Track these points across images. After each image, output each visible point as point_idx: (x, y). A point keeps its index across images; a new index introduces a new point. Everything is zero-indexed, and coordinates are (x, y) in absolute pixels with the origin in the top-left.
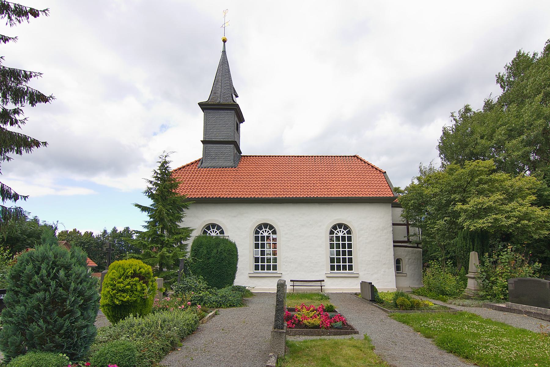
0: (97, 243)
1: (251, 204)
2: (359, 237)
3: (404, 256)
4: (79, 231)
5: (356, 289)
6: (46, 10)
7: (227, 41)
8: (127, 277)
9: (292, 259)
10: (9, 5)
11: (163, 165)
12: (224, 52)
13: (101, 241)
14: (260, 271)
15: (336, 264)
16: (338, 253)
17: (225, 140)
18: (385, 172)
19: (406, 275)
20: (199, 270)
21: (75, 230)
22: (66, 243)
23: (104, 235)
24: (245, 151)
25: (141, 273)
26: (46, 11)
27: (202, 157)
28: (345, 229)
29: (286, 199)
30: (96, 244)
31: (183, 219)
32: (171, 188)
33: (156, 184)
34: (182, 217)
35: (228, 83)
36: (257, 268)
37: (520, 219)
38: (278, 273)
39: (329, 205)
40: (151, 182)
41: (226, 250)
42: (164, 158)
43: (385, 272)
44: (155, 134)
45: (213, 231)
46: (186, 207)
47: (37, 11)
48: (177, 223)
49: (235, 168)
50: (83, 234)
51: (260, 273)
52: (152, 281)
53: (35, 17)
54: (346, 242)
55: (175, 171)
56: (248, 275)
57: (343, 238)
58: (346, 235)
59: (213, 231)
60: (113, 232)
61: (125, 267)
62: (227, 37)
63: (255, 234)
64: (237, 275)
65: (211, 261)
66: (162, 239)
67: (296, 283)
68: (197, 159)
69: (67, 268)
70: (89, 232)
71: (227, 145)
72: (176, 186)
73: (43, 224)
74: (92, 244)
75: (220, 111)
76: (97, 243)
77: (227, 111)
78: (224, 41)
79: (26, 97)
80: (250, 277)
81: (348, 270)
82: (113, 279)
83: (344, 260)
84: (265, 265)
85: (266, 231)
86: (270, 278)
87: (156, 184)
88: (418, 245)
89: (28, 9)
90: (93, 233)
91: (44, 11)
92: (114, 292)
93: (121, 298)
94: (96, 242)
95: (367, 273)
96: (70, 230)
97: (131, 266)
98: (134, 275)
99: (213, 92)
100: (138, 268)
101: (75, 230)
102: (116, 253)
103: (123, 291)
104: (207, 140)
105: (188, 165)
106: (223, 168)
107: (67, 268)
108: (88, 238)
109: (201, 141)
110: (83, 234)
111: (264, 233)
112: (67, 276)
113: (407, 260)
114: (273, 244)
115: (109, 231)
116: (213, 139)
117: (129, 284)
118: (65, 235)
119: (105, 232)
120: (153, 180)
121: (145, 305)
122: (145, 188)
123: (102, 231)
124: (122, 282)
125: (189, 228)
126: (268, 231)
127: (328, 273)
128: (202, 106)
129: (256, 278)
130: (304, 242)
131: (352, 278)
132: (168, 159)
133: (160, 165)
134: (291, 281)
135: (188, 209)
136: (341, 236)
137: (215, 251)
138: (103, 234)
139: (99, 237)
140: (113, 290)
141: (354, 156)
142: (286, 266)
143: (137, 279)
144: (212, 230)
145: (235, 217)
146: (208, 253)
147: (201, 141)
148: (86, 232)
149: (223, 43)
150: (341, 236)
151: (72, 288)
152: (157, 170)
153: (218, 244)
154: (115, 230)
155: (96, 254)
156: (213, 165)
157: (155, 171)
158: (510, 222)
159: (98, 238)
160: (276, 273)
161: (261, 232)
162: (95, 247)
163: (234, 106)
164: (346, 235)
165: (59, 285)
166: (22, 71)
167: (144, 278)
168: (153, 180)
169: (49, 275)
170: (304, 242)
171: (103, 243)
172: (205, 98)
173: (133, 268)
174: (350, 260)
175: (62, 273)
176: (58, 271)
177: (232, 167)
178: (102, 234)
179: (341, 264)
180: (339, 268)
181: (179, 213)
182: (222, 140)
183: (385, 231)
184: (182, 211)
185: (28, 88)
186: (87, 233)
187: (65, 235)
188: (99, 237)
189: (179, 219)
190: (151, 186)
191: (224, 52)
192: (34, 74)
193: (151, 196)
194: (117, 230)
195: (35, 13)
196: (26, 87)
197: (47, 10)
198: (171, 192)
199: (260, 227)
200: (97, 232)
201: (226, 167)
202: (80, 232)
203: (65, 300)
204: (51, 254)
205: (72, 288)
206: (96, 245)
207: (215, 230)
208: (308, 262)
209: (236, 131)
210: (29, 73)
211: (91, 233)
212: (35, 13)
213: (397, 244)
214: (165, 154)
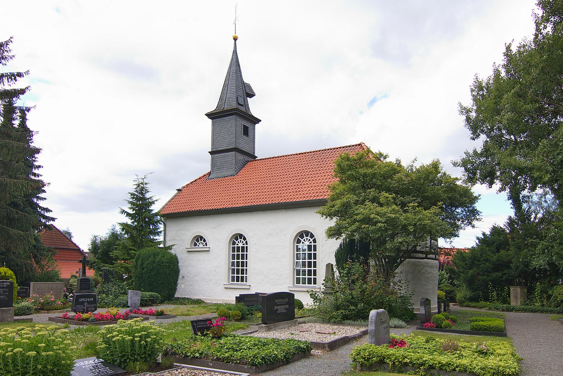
1: (258, 212)
6: (28, 87)
7: (238, 39)
9: (259, 271)
12: (235, 52)
14: (301, 285)
19: (248, 287)
24: (260, 153)
29: (251, 207)
35: (234, 86)
38: (317, 287)
39: (294, 211)
44: (362, 113)
62: (237, 35)
63: (232, 245)
77: (229, 117)
78: (235, 39)
80: (225, 288)
84: (300, 278)
111: (305, 241)
114: (304, 255)
127: (226, 284)
128: (209, 115)
129: (230, 289)
131: (232, 289)
136: (241, 247)
141: (359, 145)
142: (254, 278)
144: (305, 238)
149: (234, 41)
150: (241, 247)
163: (234, 111)
164: (312, 244)
172: (212, 107)
191: (235, 52)
201: (227, 176)
208: (273, 274)
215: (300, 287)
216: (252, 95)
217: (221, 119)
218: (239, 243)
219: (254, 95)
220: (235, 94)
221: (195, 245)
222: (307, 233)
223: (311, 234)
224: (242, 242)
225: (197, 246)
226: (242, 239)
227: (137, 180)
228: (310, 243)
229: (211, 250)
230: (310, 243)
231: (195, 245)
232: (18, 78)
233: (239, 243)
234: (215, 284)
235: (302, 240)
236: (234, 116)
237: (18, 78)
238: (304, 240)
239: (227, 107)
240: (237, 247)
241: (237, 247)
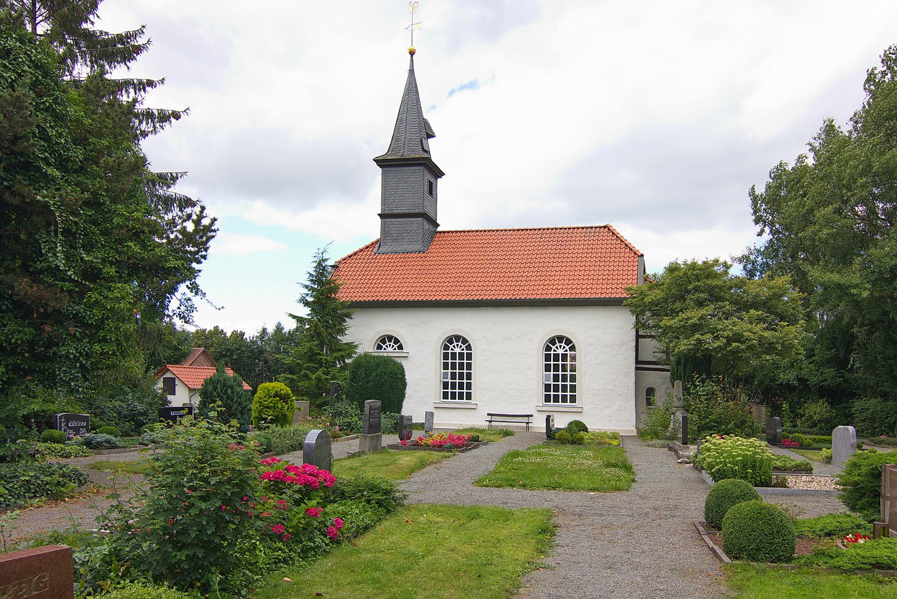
0: (252, 351)
2: (585, 356)
3: (659, 385)
4: (222, 331)
5: (628, 436)
8: (270, 397)
9: (491, 385)
10: (153, 112)
11: (319, 264)
12: (412, 71)
13: (257, 348)
14: (449, 400)
15: (552, 393)
16: (556, 378)
17: (410, 211)
18: (642, 255)
20: (357, 395)
21: (216, 328)
22: (204, 352)
23: (263, 338)
24: (445, 223)
25: (281, 394)
26: (187, 111)
27: (379, 237)
30: (249, 352)
31: (346, 332)
32: (330, 293)
33: (313, 289)
34: (346, 329)
36: (445, 396)
37: (730, 340)
40: (307, 287)
41: (388, 372)
42: (320, 255)
43: (620, 406)
45: (390, 345)
46: (349, 316)
47: (179, 112)
48: (338, 337)
49: (424, 252)
50: (229, 334)
51: (464, 403)
52: (291, 401)
53: (177, 119)
54: (465, 371)
55: (344, 260)
57: (564, 357)
59: (390, 345)
60: (276, 332)
61: (270, 388)
62: (415, 47)
64: (405, 404)
65: (370, 385)
66: (319, 357)
67: (494, 418)
68: (374, 240)
69: (232, 387)
70: (239, 332)
71: (413, 219)
72: (336, 289)
73: (181, 330)
74: (243, 352)
75: (403, 168)
76: (252, 350)
77: (413, 168)
78: (412, 53)
79: (175, 205)
81: (570, 402)
82: (260, 398)
83: (564, 388)
85: (457, 345)
86: (462, 410)
87: (313, 289)
89: (170, 112)
90: (244, 333)
91: (185, 111)
92: (261, 407)
94: (250, 349)
95: (595, 408)
96: (209, 327)
97: (273, 388)
98: (276, 395)
99: (395, 138)
100: (279, 390)
101: (216, 328)
102: (283, 369)
103: (268, 407)
105: (361, 250)
106: (408, 253)
107: (232, 387)
108: (237, 342)
109: (379, 215)
110: (229, 334)
112: (232, 392)
113: (663, 390)
115: (271, 330)
117: (271, 402)
118: (203, 337)
119: (264, 330)
120: (308, 283)
121: (286, 420)
122: (299, 297)
123: (260, 329)
124: (266, 401)
125: (353, 343)
126: (461, 346)
128: (381, 162)
129: (443, 409)
130: (507, 362)
132: (325, 256)
133: (315, 265)
134: (489, 414)
135: (351, 318)
136: (459, 353)
137: (374, 373)
138: (261, 335)
139: (255, 339)
140: (260, 406)
141: (605, 227)
143: (278, 398)
144: (388, 344)
145: (416, 326)
146: (367, 375)
147: (379, 215)
148: (235, 331)
151: (235, 400)
152: (312, 273)
153: (378, 365)
154: (279, 328)
155: (250, 371)
156: (394, 249)
157: (309, 273)
158: (717, 344)
159: (253, 342)
160: (470, 404)
161: (451, 347)
162: (248, 357)
163: (423, 160)
164: (465, 351)
165: (228, 398)
166: (169, 174)
167: (284, 398)
168: (308, 283)
169: (221, 392)
170: (507, 362)
171: (261, 351)
172: (382, 148)
173: (275, 389)
174: (469, 386)
175: (229, 391)
176: (227, 389)
177: (420, 252)
178: (259, 335)
179: (457, 391)
180: (453, 396)
181: (341, 324)
182: (406, 211)
183: (624, 347)
184: (345, 321)
185: (175, 194)
186: (234, 333)
187: (203, 337)
188: (255, 339)
189: (342, 331)
190: (306, 291)
191: (412, 71)
192: (180, 175)
193: (307, 304)
194: (283, 328)
195: (177, 116)
196: (174, 194)
197: (188, 109)
198: (330, 297)
199: (450, 340)
200: (251, 332)
201: (411, 252)
202: (225, 331)
203: (231, 407)
204: (221, 379)
205: (235, 400)
206: (249, 354)
207: (392, 344)
209: (427, 195)
210: (175, 175)
211: (242, 334)
212: (177, 116)
213: (641, 365)
214: (320, 251)
215: (558, 406)
216: (430, 135)
217: (399, 169)
218: (558, 349)
219: (434, 137)
220: (418, 135)
221: (379, 347)
222: (458, 338)
223: (464, 338)
224: (459, 346)
225: (383, 350)
226: (461, 342)
227: (317, 255)
228: (565, 351)
229: (410, 355)
230: (565, 351)
231: (379, 347)
232: (148, 89)
233: (558, 349)
234: (418, 402)
235: (384, 346)
236: (422, 168)
237: (148, 89)
238: (454, 346)
239: (408, 155)
240: (554, 354)
241: (554, 354)
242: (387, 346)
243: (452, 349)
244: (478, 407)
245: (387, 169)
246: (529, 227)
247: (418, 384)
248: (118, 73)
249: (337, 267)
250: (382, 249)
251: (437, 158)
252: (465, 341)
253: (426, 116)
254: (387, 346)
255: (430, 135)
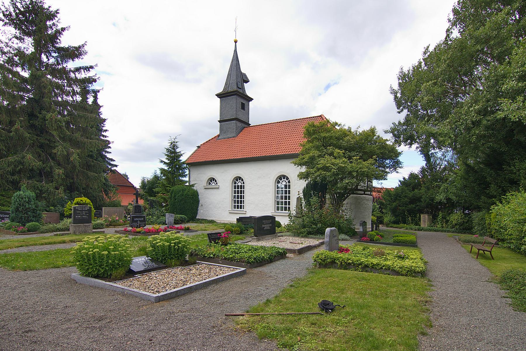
12: (235, 51)
19: (245, 213)
24: (253, 121)
27: (218, 133)
28: (284, 178)
44: (320, 94)
56: (228, 212)
58: (288, 184)
75: (228, 97)
77: (232, 97)
78: (236, 42)
88: (364, 193)
93: (69, 212)
104: (222, 119)
116: (225, 119)
126: (286, 181)
128: (218, 95)
130: (259, 190)
141: (320, 116)
145: (223, 173)
164: (288, 184)
170: (259, 190)
172: (220, 90)
182: (229, 118)
191: (235, 51)
216: (247, 81)
219: (249, 81)
221: (210, 184)
222: (284, 177)
232: (91, 69)
235: (281, 181)
236: (235, 96)
237: (91, 69)
242: (282, 181)
243: (238, 184)
244: (247, 213)
245: (223, 99)
246: (279, 122)
247: (223, 201)
248: (71, 65)
249: (200, 147)
250: (220, 138)
251: (249, 93)
252: (287, 178)
253: (243, 71)
254: (282, 181)
255: (247, 81)
